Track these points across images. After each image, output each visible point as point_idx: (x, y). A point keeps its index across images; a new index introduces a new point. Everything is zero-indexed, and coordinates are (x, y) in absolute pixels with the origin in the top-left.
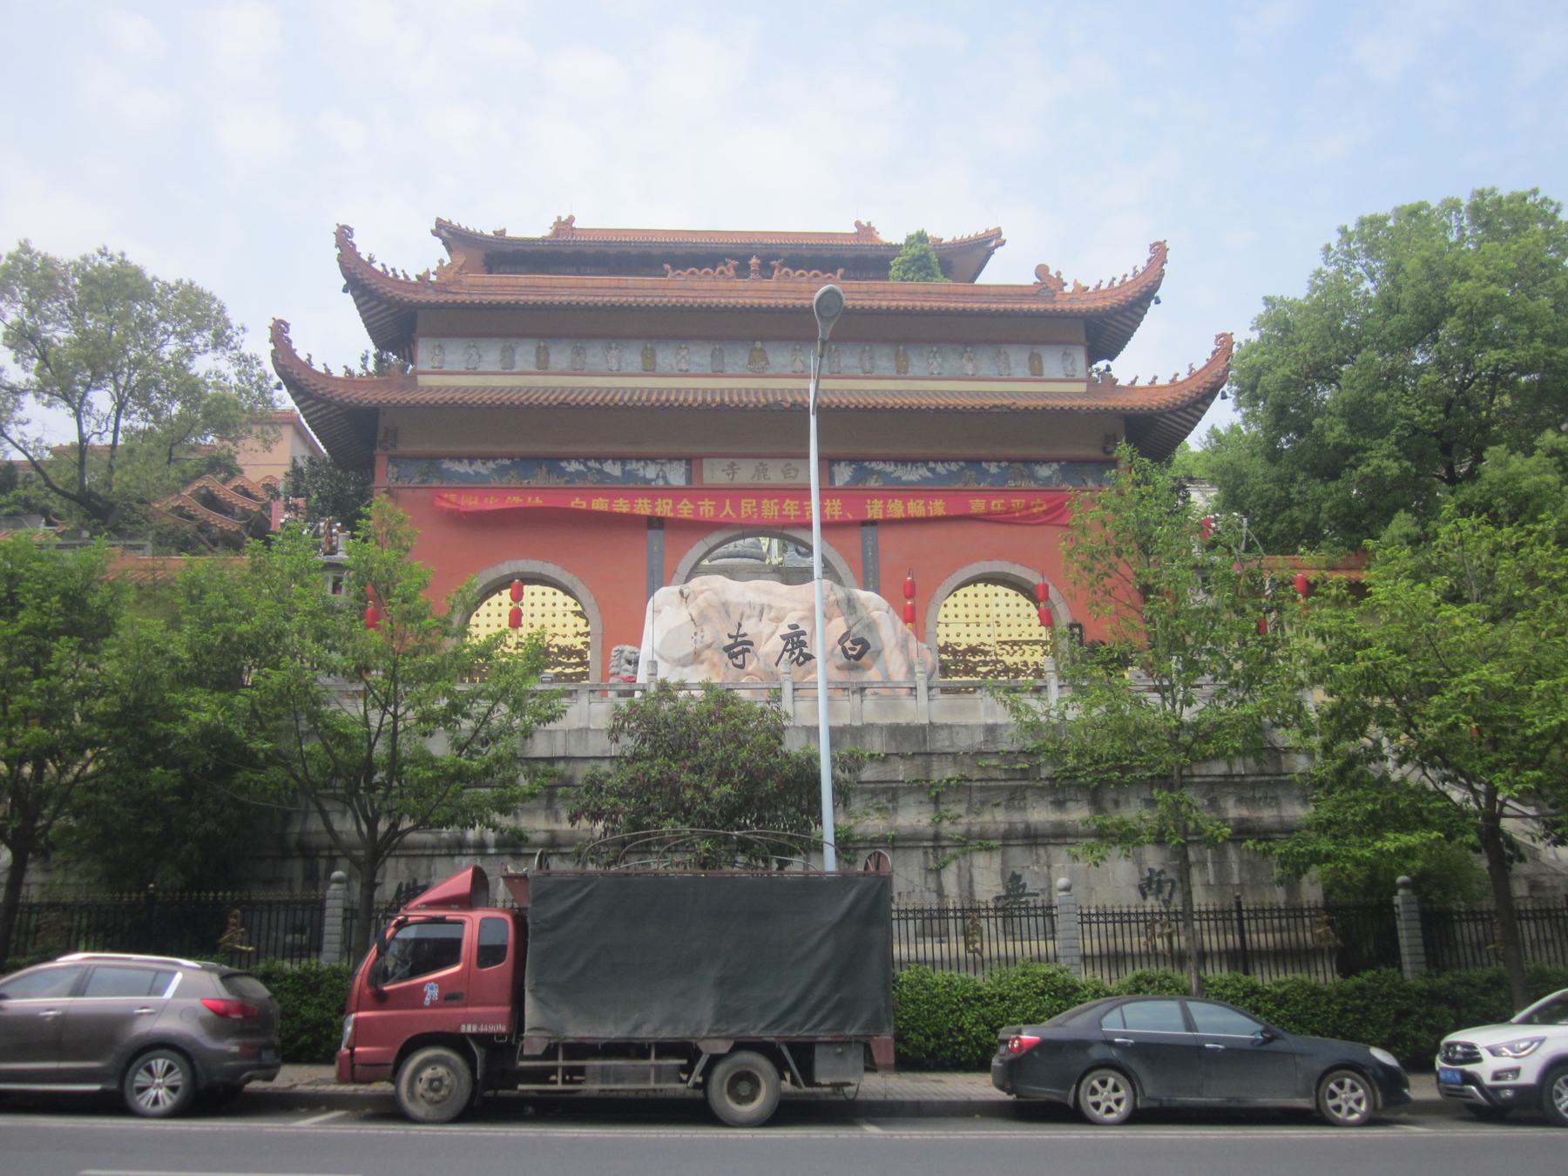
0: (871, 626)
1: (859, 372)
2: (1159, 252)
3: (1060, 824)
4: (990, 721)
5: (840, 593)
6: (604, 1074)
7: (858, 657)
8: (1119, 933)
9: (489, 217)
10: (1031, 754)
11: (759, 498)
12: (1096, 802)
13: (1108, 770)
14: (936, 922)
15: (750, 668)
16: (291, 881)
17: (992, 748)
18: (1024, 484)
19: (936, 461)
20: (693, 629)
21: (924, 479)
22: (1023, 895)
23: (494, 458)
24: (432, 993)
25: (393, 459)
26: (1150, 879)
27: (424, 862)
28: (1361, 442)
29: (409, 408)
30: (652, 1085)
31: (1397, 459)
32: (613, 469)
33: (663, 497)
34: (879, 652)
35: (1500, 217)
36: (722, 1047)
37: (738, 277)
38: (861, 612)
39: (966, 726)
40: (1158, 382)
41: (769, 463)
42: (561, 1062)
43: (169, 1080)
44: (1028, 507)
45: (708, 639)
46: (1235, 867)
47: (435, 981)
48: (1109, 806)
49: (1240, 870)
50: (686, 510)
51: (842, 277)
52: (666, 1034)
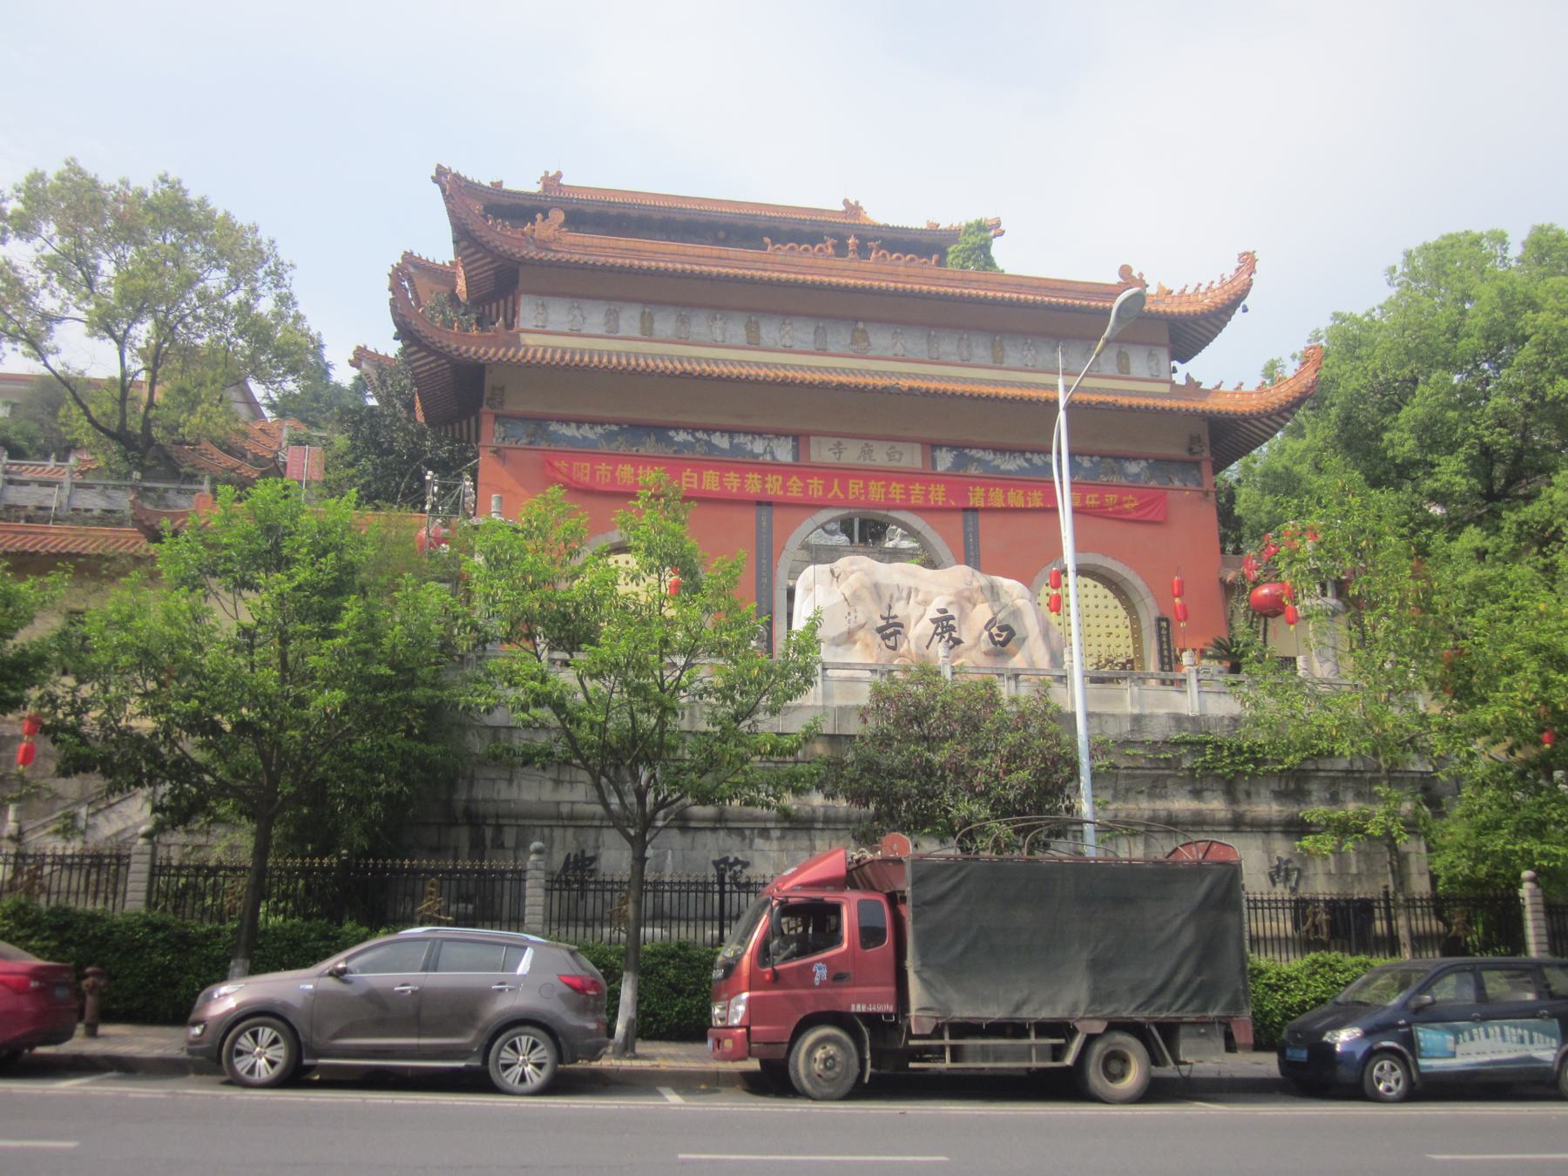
0: (1016, 613)
1: (956, 359)
2: (1248, 262)
3: (1198, 813)
4: (1136, 711)
5: (981, 580)
6: (985, 1053)
7: (1003, 644)
10: (1177, 744)
12: (1230, 794)
13: (1243, 763)
15: (902, 650)
16: (456, 849)
17: (1137, 737)
18: (1115, 480)
19: (1032, 452)
21: (1021, 469)
23: (602, 424)
24: (821, 973)
25: (497, 418)
26: (1278, 867)
27: (592, 833)
28: (1429, 457)
31: (1465, 475)
32: (722, 441)
33: (773, 473)
34: (1024, 639)
36: (1098, 1027)
37: (838, 255)
38: (1004, 599)
39: (1113, 715)
40: (1244, 389)
41: (875, 445)
43: (533, 1057)
44: (1120, 503)
45: (861, 619)
47: (823, 961)
48: (1241, 796)
50: (795, 488)
52: (1045, 1014)
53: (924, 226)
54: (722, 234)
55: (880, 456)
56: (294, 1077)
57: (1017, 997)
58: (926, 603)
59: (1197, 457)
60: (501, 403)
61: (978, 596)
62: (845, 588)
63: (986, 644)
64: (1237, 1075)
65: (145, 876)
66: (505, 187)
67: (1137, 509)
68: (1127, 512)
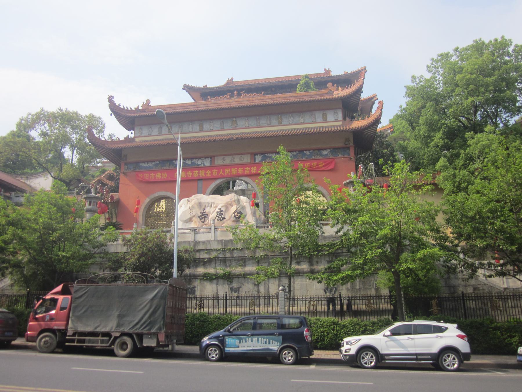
0: (244, 208)
1: (266, 125)
3: (298, 269)
6: (89, 341)
9: (199, 82)
11: (199, 170)
12: (311, 263)
15: (206, 223)
18: (317, 157)
23: (154, 162)
25: (126, 164)
29: (132, 148)
33: (202, 170)
36: (118, 334)
38: (241, 203)
41: (235, 157)
42: (76, 337)
44: (318, 165)
45: (194, 214)
48: (315, 263)
49: (359, 284)
53: (343, 73)
54: (273, 89)
55: (237, 160)
57: (96, 325)
58: (216, 207)
59: (348, 146)
60: (126, 159)
61: (234, 203)
62: (190, 205)
63: (233, 218)
66: (208, 86)
67: (324, 166)
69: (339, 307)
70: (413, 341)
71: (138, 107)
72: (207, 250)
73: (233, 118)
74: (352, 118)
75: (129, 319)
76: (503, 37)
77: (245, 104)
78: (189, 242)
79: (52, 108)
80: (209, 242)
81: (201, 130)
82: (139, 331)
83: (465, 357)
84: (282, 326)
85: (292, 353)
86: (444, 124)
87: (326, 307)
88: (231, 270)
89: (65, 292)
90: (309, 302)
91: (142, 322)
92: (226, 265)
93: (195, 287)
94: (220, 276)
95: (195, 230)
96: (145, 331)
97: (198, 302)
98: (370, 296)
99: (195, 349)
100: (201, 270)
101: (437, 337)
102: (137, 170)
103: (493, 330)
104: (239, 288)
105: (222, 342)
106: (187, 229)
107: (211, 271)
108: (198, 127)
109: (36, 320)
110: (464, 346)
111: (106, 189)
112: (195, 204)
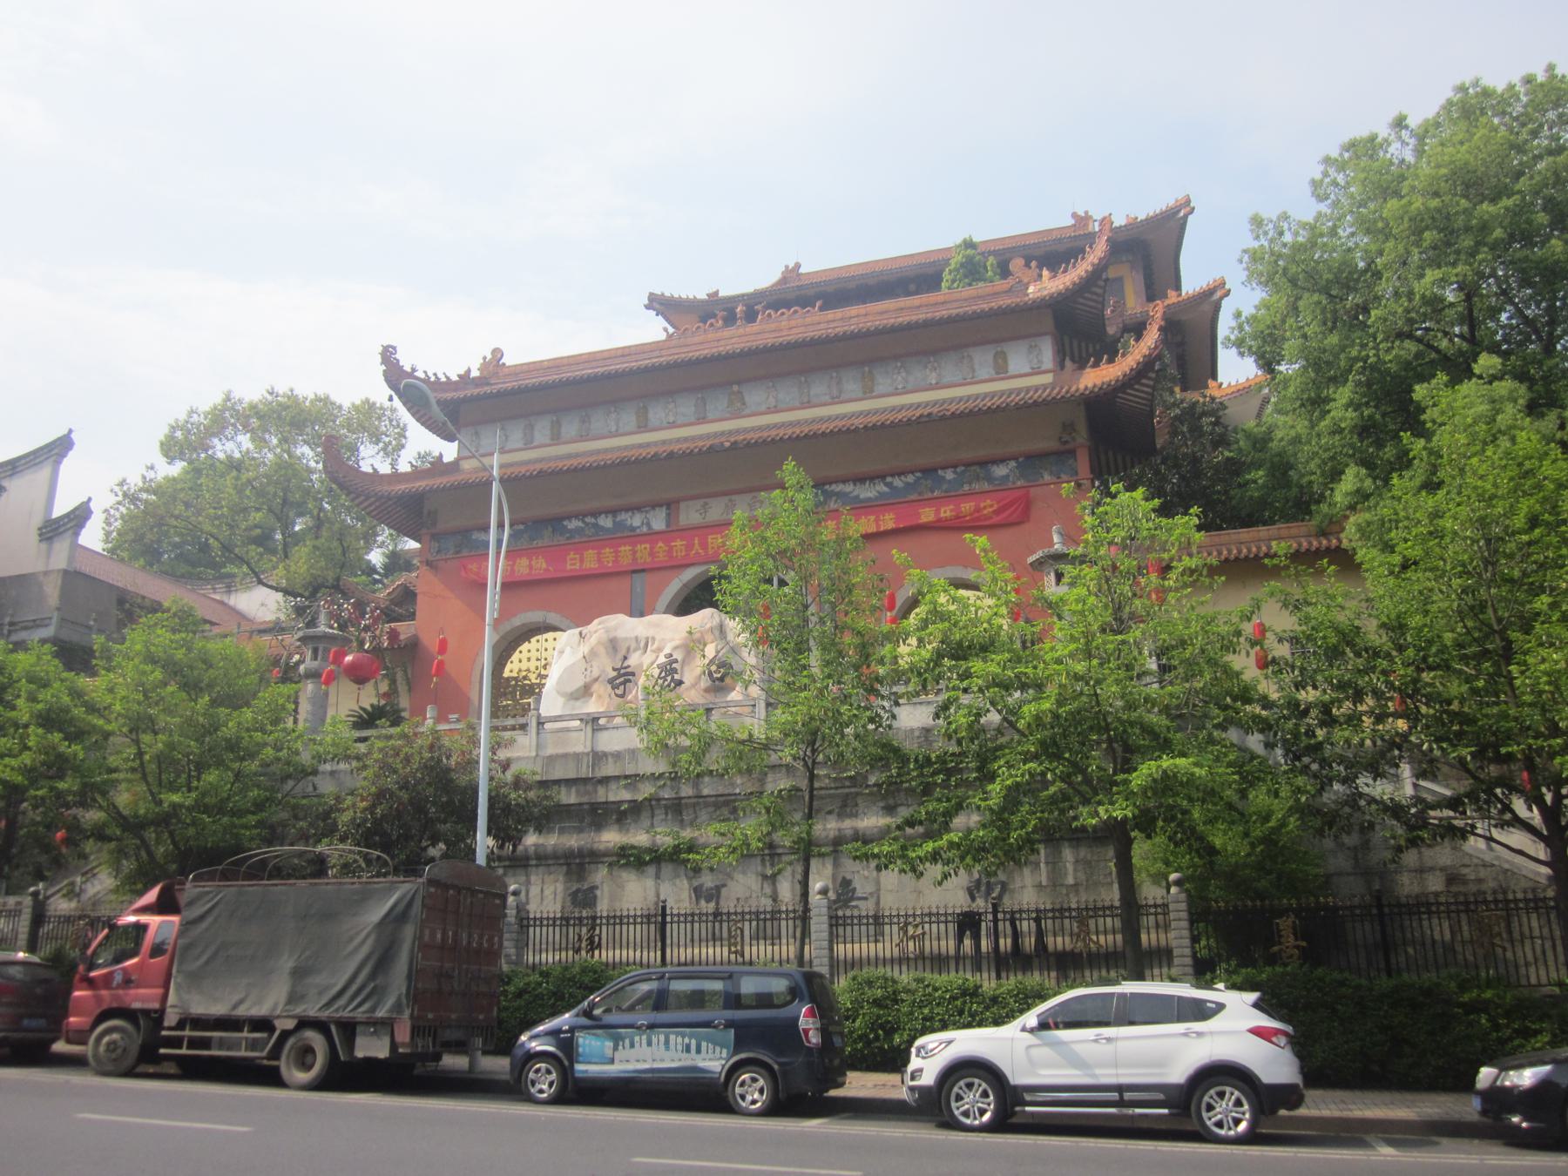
1: (827, 398)
6: (222, 1044)
8: (943, 935)
11: (634, 544)
14: (769, 924)
19: (892, 475)
20: (584, 665)
21: (882, 495)
22: (852, 899)
30: (243, 1053)
32: (606, 522)
35: (1471, 106)
36: (290, 1024)
42: (187, 1033)
44: (978, 510)
45: (596, 673)
46: (1070, 867)
49: (1075, 870)
51: (821, 309)
56: (1004, 1122)
57: (236, 998)
58: (660, 650)
61: (709, 637)
62: (585, 649)
63: (705, 682)
64: (1466, 1141)
65: (825, 927)
66: (721, 294)
67: (997, 512)
68: (987, 518)
69: (1009, 941)
70: (1110, 1047)
71: (469, 371)
72: (626, 777)
73: (731, 384)
74: (1081, 365)
75: (318, 980)
76: (1551, 68)
77: (770, 339)
78: (577, 757)
79: (251, 392)
80: (633, 752)
81: (643, 427)
82: (346, 1014)
83: (1286, 1096)
84: (734, 1000)
85: (761, 1082)
86: (1356, 359)
87: (952, 943)
88: (696, 834)
89: (165, 905)
90: (904, 929)
91: (354, 988)
92: (682, 821)
93: (596, 887)
94: (663, 854)
95: (595, 720)
96: (360, 1014)
97: (584, 930)
98: (1087, 909)
99: (497, 1065)
100: (611, 838)
101: (1185, 1035)
102: (465, 553)
103: (1467, 1013)
104: (718, 888)
105: (567, 1044)
106: (572, 717)
107: (639, 838)
108: (634, 418)
109: (91, 983)
110: (1274, 1064)
111: (372, 612)
112: (599, 643)
